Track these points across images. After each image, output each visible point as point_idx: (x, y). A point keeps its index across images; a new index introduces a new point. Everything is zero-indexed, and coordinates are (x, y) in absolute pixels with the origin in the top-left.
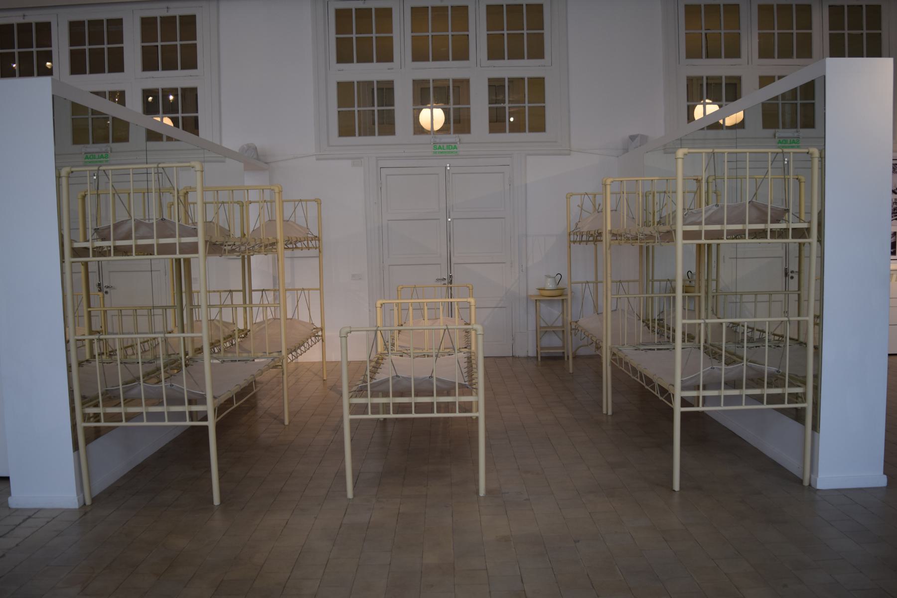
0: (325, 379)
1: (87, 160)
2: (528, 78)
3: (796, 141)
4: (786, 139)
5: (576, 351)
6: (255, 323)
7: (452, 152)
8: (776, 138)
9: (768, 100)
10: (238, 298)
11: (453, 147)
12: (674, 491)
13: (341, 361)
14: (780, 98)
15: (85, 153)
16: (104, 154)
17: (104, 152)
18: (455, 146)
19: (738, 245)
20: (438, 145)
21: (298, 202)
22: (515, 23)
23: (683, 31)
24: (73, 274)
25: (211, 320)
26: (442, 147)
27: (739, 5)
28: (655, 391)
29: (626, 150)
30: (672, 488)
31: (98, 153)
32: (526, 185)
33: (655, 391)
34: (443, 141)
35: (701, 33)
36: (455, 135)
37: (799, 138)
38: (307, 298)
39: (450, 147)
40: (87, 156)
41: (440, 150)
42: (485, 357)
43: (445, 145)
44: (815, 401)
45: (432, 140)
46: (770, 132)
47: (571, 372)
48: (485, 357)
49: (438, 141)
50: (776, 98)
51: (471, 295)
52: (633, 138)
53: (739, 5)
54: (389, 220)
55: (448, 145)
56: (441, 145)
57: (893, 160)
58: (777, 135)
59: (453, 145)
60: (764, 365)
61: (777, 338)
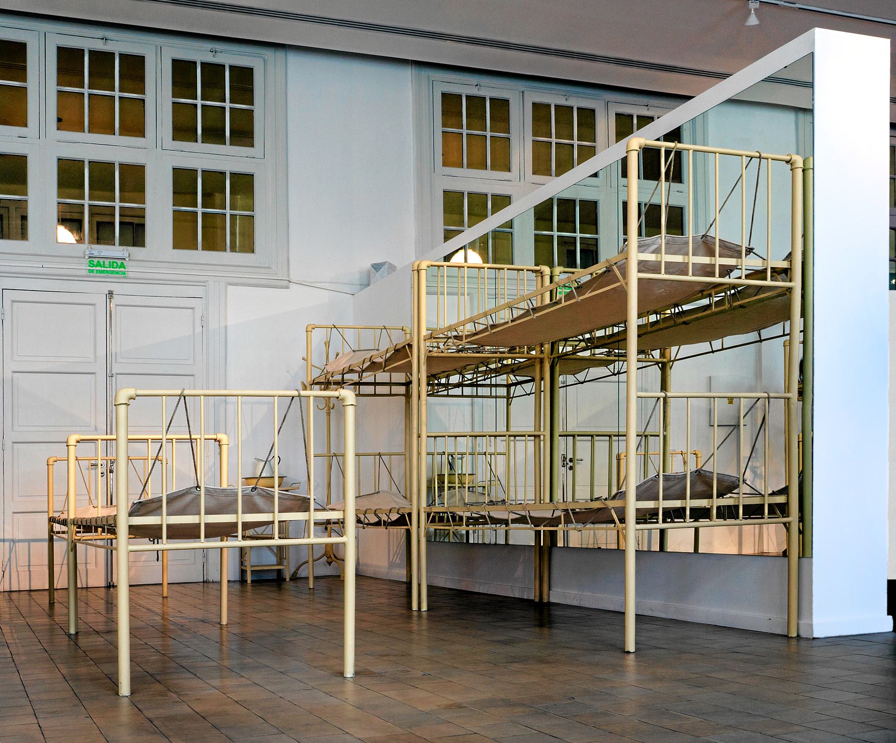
7: (117, 273)
10: (565, 385)
12: (628, 652)
20: (96, 260)
22: (565, 128)
23: (439, 129)
26: (102, 263)
29: (366, 284)
30: (624, 648)
32: (226, 327)
34: (104, 254)
35: (486, 136)
36: (122, 248)
41: (99, 268)
42: (130, 586)
43: (107, 262)
44: (568, 613)
45: (87, 253)
47: (312, 587)
48: (130, 586)
49: (96, 254)
52: (377, 267)
54: (14, 372)
55: (112, 261)
56: (101, 261)
57: (427, 330)
59: (119, 262)
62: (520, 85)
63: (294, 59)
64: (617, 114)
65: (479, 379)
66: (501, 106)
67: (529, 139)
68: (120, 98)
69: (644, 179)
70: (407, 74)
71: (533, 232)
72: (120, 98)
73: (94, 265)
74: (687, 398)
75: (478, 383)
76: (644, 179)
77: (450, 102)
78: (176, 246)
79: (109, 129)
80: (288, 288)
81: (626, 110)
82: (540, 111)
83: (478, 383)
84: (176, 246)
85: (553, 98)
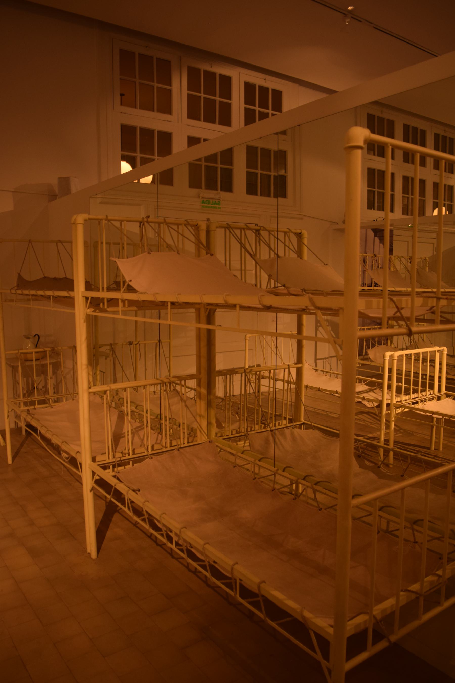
1: (204, 204)
3: (217, 203)
4: (209, 200)
6: (233, 396)
8: (201, 198)
9: (193, 161)
11: (214, 202)
14: (203, 160)
15: (202, 198)
16: (217, 201)
17: (218, 199)
18: (215, 201)
25: (233, 396)
27: (170, 62)
28: (125, 507)
31: (213, 199)
33: (125, 507)
37: (220, 200)
38: (280, 356)
39: (207, 202)
40: (203, 200)
46: (194, 191)
50: (200, 160)
51: (102, 383)
53: (170, 62)
58: (201, 195)
61: (128, 427)
68: (157, 87)
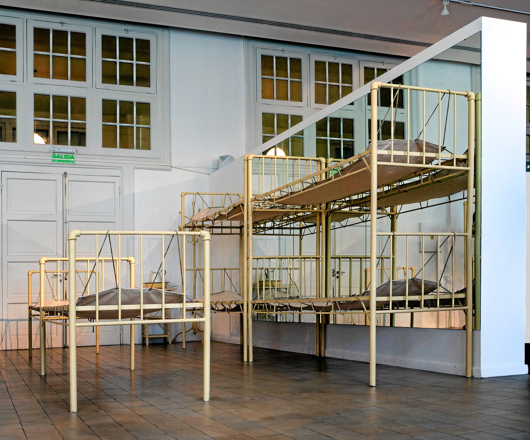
0: (98, 352)
2: (102, 57)
5: (176, 337)
7: (69, 161)
13: (413, 327)
19: (298, 166)
20: (57, 154)
21: (156, 281)
23: (260, 76)
24: (28, 302)
26: (60, 156)
29: (217, 168)
32: (134, 194)
34: (61, 150)
36: (72, 147)
41: (58, 159)
42: (77, 347)
43: (63, 155)
45: (52, 150)
48: (77, 347)
49: (57, 150)
52: (223, 158)
54: (8, 220)
55: (66, 154)
56: (60, 154)
59: (70, 155)
60: (269, 286)
62: (308, 50)
63: (174, 35)
64: (365, 68)
65: (283, 225)
66: (296, 63)
67: (313, 82)
68: (71, 58)
69: (381, 106)
70: (241, 44)
71: (315, 137)
72: (71, 58)
73: (55, 157)
74: (407, 236)
75: (283, 227)
76: (381, 106)
77: (266, 60)
78: (104, 146)
79: (65, 77)
80: (170, 170)
81: (370, 65)
82: (319, 66)
83: (283, 227)
84: (104, 146)
85: (327, 58)
